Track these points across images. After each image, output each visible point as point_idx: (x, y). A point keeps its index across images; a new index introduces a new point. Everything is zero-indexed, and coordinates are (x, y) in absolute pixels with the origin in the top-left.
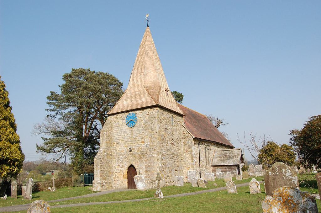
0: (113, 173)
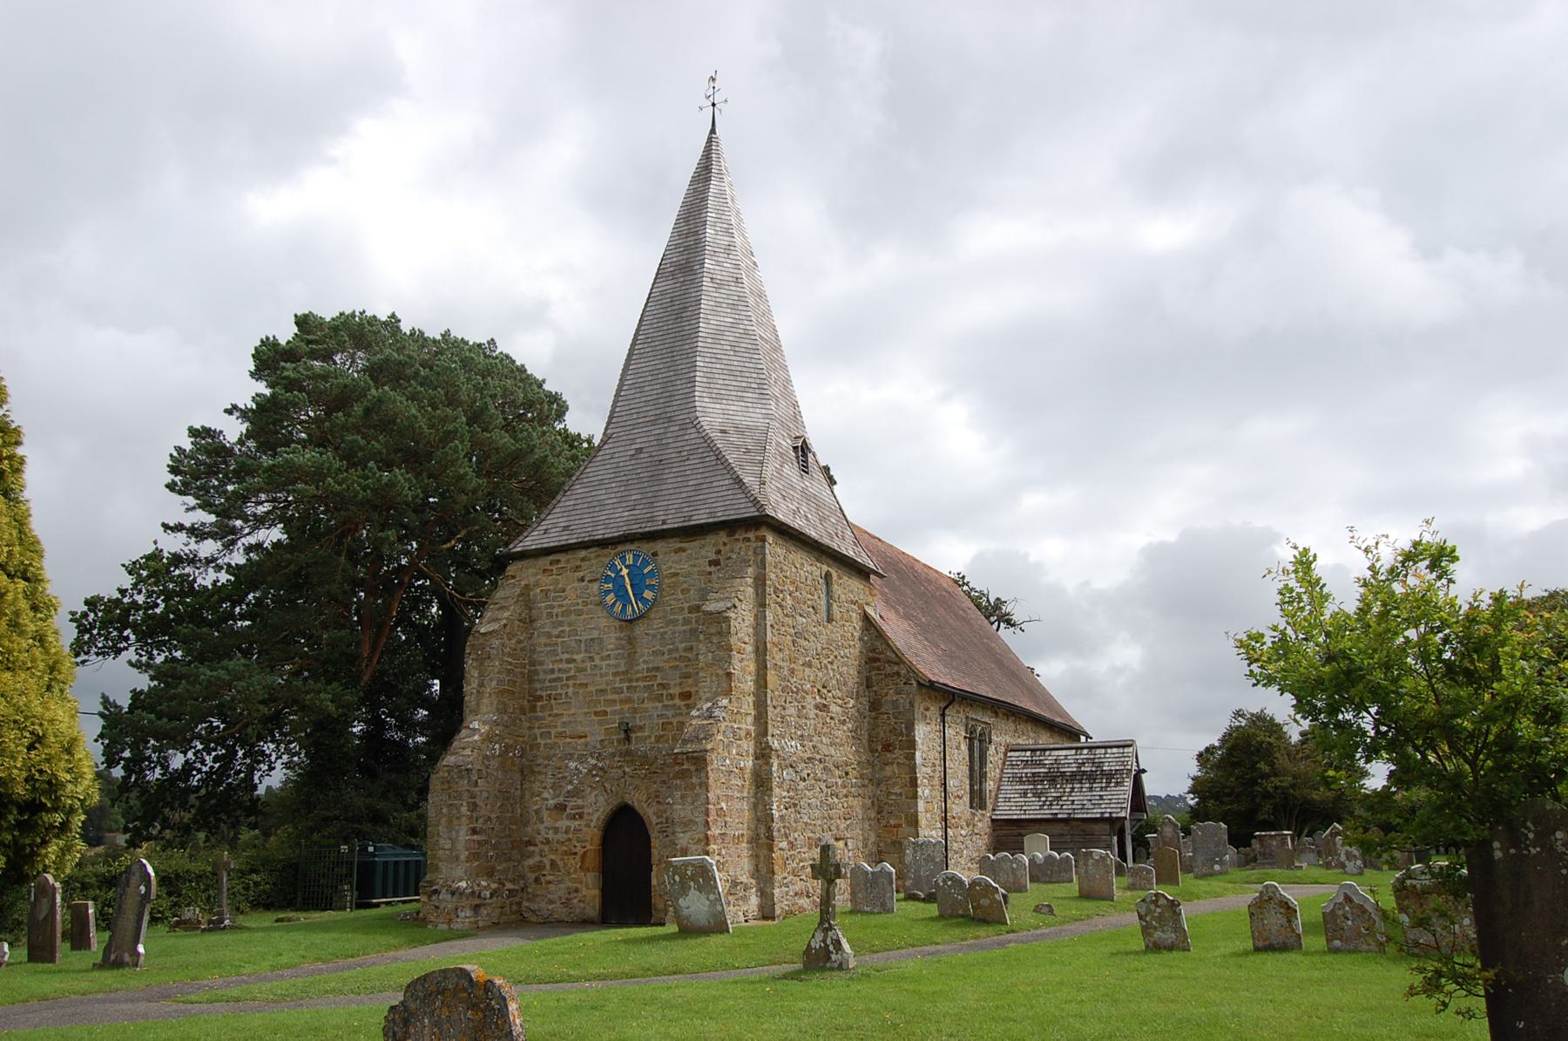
0: (530, 843)
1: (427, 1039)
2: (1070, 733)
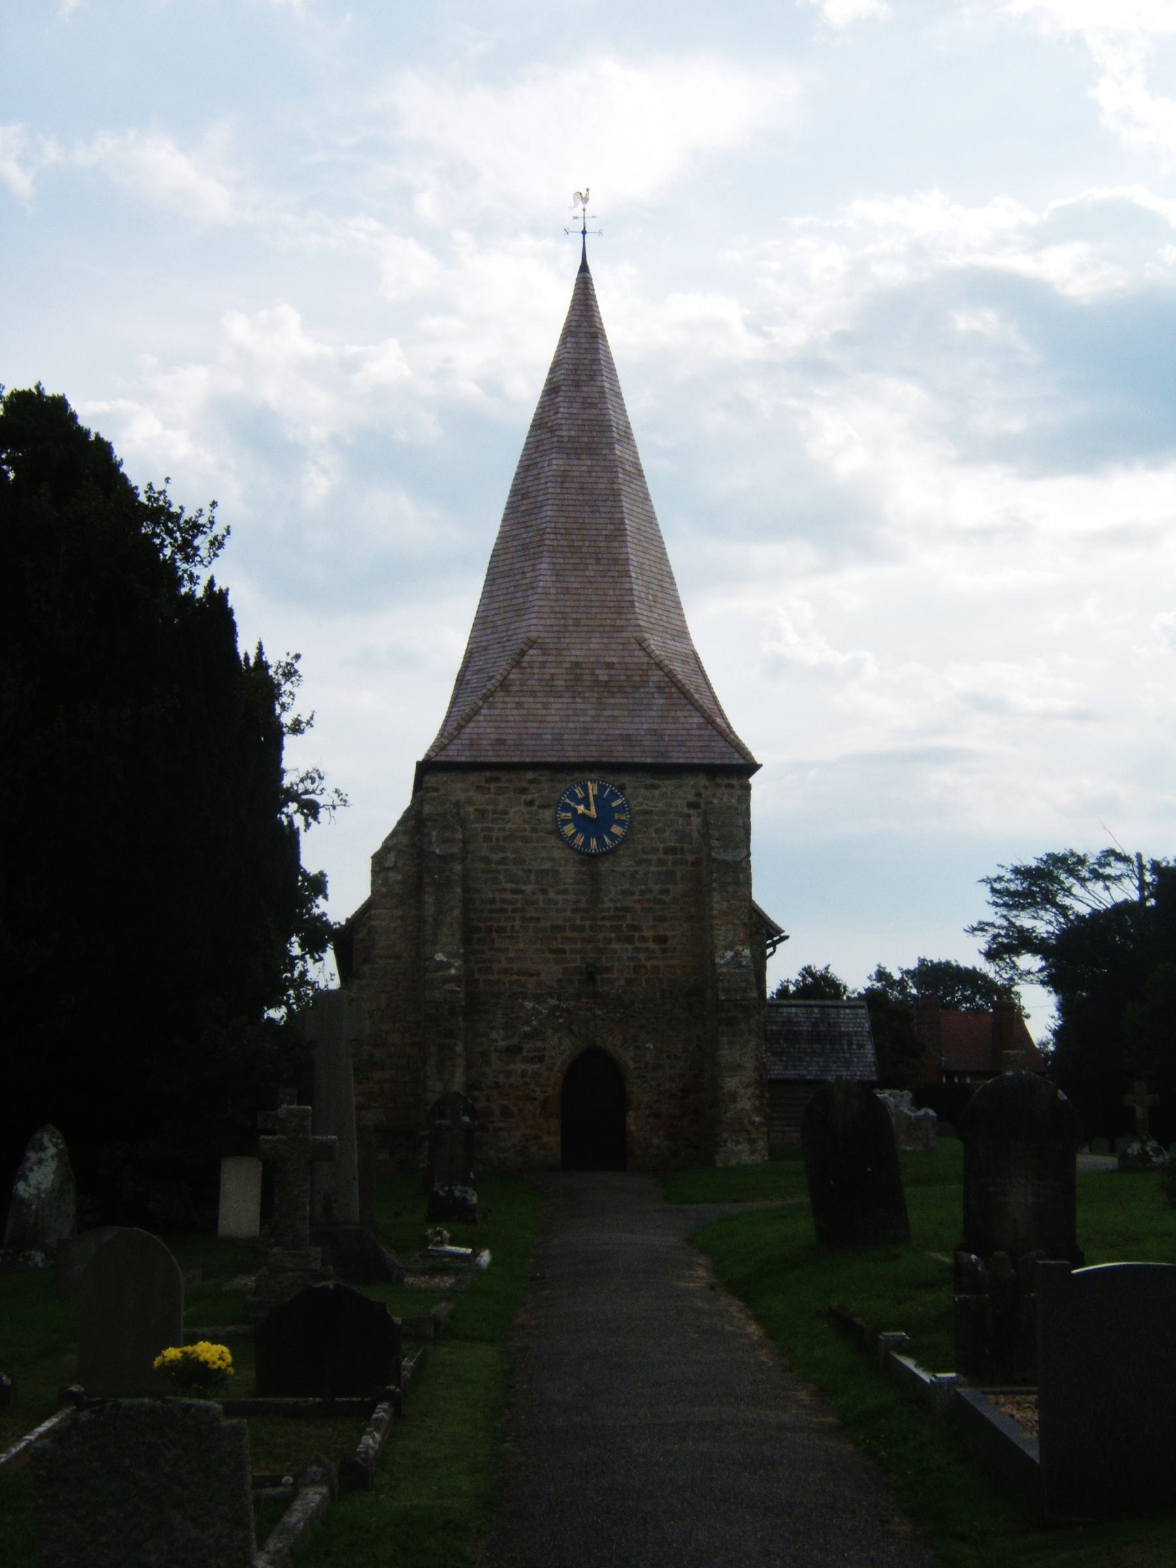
1: (2, 1252)
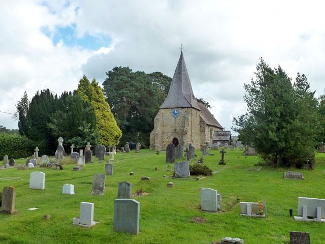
2: (222, 129)
